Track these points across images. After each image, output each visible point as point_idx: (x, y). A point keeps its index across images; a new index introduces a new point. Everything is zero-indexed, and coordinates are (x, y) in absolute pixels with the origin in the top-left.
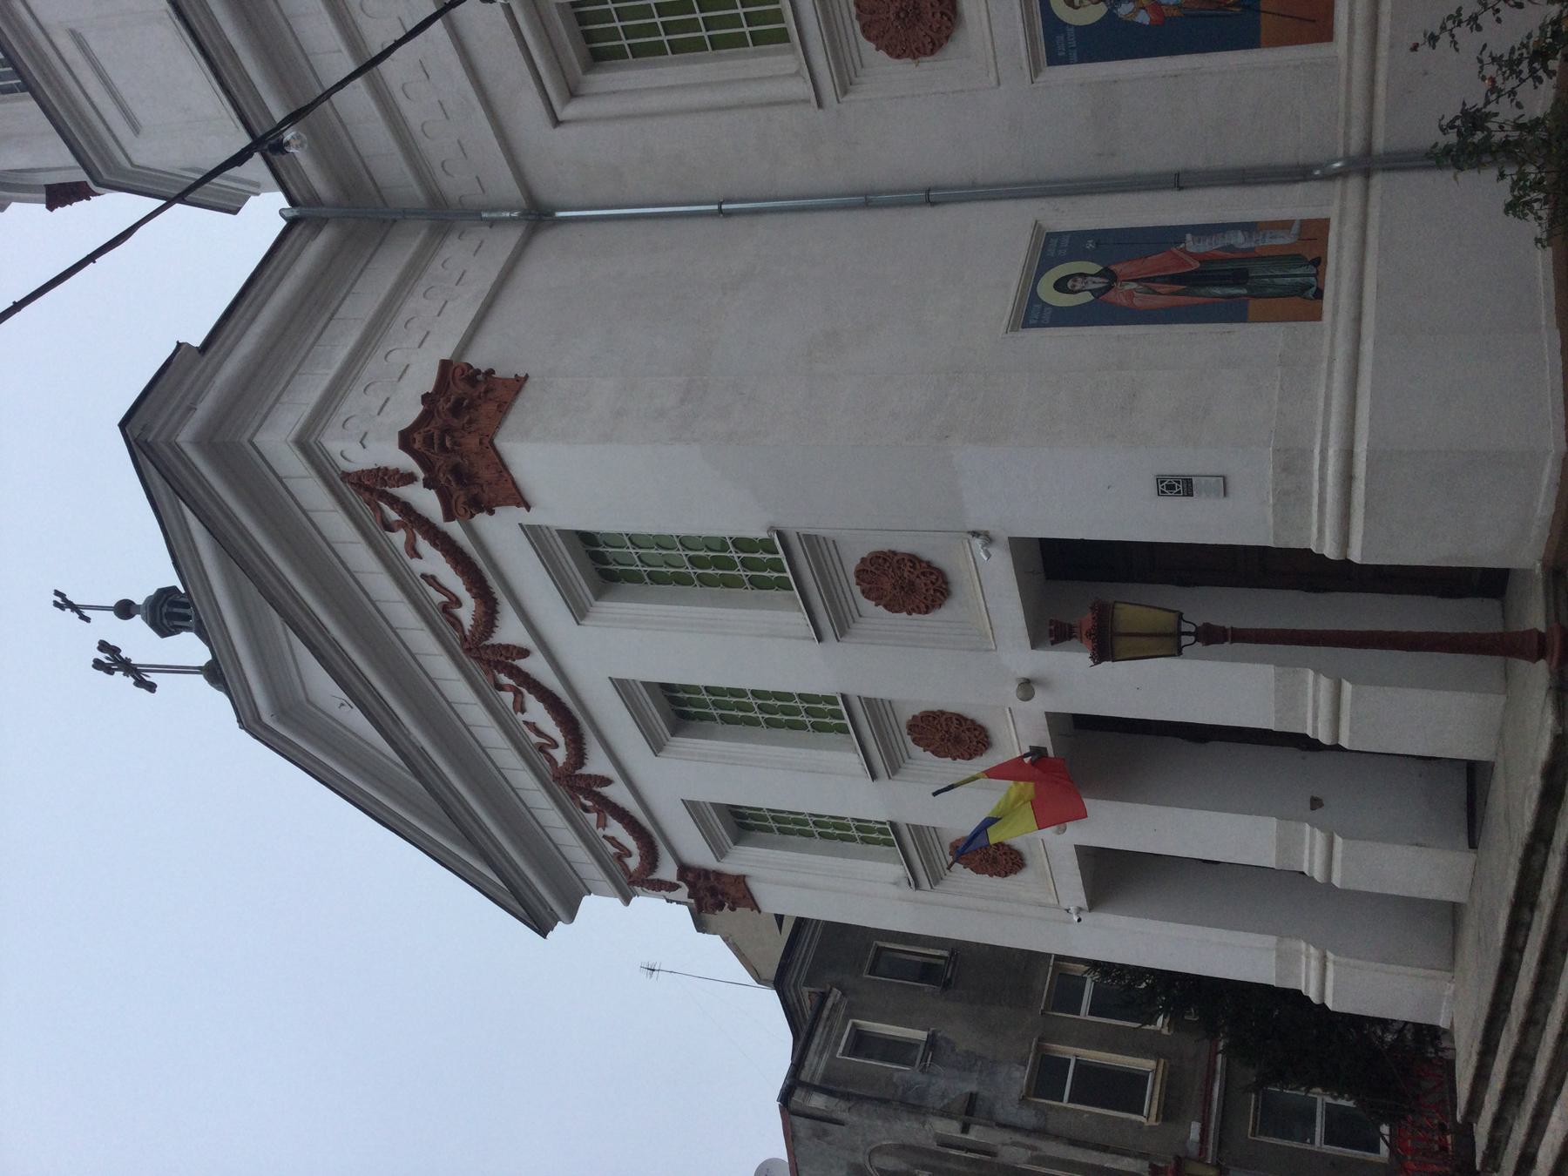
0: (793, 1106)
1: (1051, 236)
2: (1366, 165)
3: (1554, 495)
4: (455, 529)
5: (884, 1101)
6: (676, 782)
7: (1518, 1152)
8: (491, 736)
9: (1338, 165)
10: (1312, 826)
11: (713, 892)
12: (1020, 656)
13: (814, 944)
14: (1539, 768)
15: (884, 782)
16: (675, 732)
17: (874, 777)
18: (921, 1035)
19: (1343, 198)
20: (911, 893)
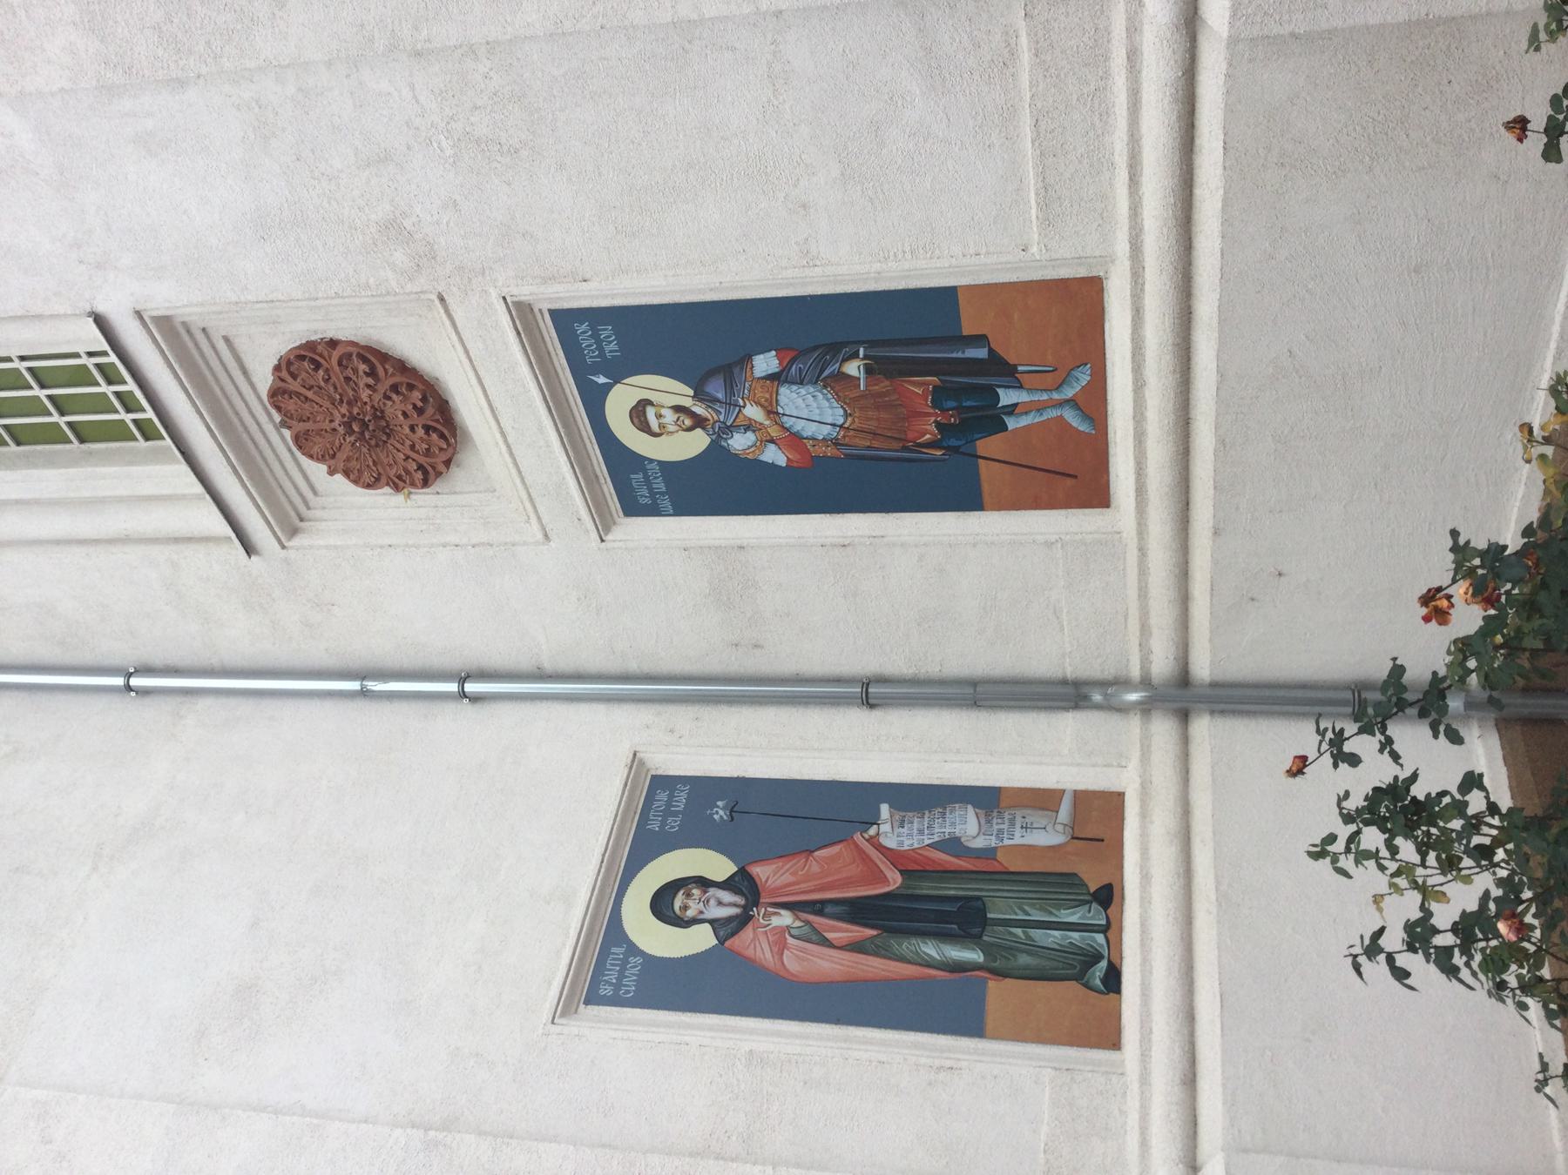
1: (662, 783)
2: (1181, 697)
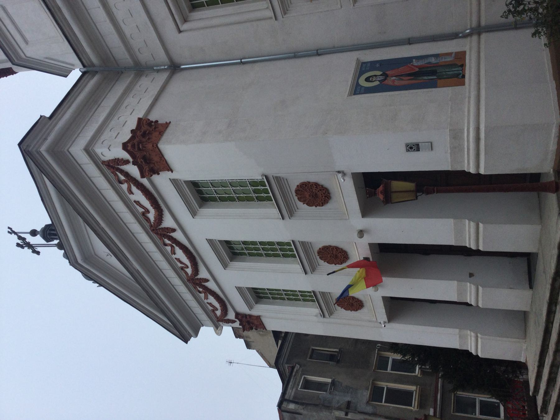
0: (283, 408)
1: (363, 63)
2: (479, 30)
3: (556, 140)
4: (145, 181)
5: (316, 405)
6: (233, 279)
7: (554, 404)
8: (163, 264)
9: (468, 31)
10: (470, 283)
11: (249, 323)
12: (359, 222)
13: (289, 350)
14: (557, 245)
15: (310, 276)
16: (232, 260)
17: (306, 273)
18: (329, 380)
19: (471, 42)
20: (322, 319)
